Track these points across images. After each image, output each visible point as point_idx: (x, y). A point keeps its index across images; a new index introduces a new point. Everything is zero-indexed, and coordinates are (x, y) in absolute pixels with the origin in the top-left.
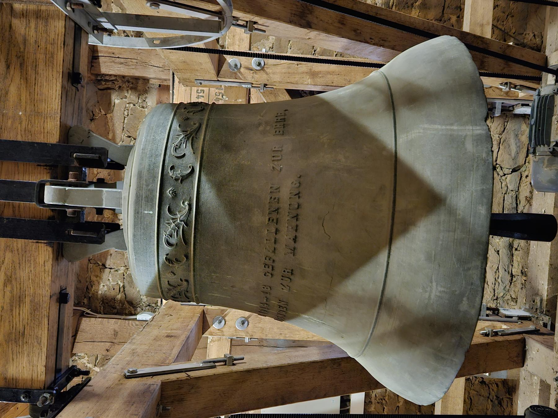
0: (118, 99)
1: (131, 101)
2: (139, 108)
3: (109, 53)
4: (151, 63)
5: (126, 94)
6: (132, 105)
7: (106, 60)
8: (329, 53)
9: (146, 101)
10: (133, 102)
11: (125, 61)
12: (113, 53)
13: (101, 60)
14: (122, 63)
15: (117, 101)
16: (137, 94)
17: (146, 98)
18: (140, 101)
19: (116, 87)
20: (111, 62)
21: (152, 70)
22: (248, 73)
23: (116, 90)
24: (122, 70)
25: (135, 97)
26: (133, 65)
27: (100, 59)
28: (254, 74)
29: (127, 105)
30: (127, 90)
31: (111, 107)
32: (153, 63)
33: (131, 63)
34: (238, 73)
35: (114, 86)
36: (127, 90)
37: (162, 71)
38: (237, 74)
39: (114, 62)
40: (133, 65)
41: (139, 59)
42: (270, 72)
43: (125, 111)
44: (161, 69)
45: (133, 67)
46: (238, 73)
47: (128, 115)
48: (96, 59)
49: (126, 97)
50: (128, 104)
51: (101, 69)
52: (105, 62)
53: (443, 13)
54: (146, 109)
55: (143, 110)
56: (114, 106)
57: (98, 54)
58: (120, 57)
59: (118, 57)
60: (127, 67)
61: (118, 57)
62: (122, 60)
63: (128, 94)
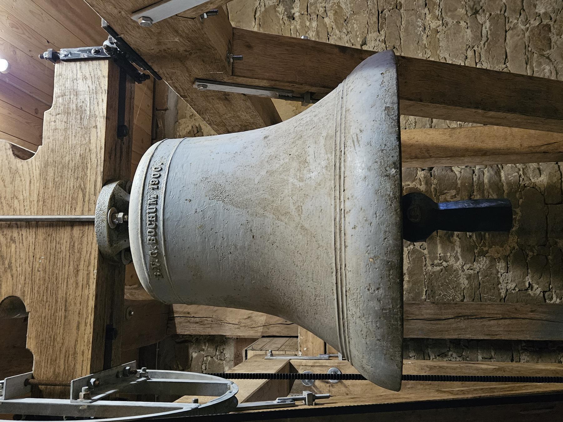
0: (196, 352)
1: (208, 354)
2: (216, 360)
3: (185, 313)
4: (226, 320)
5: (203, 348)
6: (209, 358)
7: (181, 320)
8: (418, 290)
9: (224, 352)
10: (210, 354)
11: (201, 321)
12: (189, 313)
13: (177, 320)
14: (197, 323)
15: (194, 355)
16: (214, 347)
17: (223, 349)
18: (217, 353)
19: (193, 339)
20: (187, 322)
21: (227, 328)
22: (324, 386)
23: (193, 342)
24: (198, 330)
25: (212, 349)
26: (208, 324)
27: (175, 320)
28: (331, 388)
29: (205, 358)
30: (205, 343)
31: (188, 362)
32: (228, 320)
33: (206, 322)
34: (312, 387)
35: (191, 338)
36: (205, 343)
37: (238, 328)
38: (311, 388)
39: (189, 321)
40: (208, 324)
41: (214, 317)
42: (349, 384)
43: (202, 364)
44: (237, 326)
45: (209, 326)
46: (312, 387)
47: (206, 369)
48: (171, 320)
49: (203, 350)
50: (206, 357)
51: (177, 330)
52: (180, 323)
53: (547, 237)
54: (224, 362)
55: (221, 362)
56: (192, 360)
57: (174, 315)
58: (195, 316)
59: (193, 317)
60: (203, 326)
61: (193, 317)
62: (198, 320)
63: (205, 346)
